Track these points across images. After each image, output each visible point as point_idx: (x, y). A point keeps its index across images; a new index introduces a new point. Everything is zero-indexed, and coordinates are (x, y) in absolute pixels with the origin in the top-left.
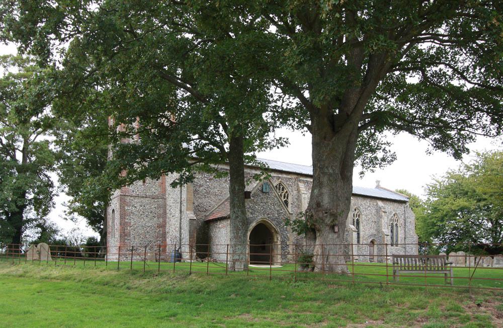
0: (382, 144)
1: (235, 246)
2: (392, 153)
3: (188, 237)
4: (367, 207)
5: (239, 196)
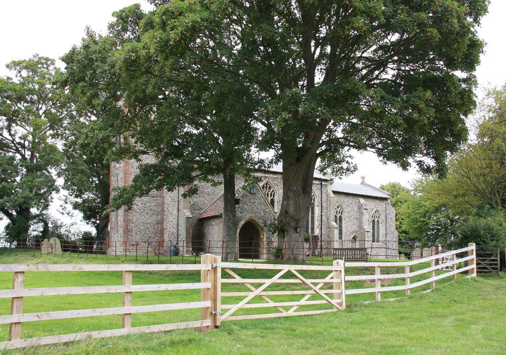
0: (346, 157)
1: (228, 241)
2: (354, 164)
3: (185, 233)
4: (349, 204)
5: (231, 200)
